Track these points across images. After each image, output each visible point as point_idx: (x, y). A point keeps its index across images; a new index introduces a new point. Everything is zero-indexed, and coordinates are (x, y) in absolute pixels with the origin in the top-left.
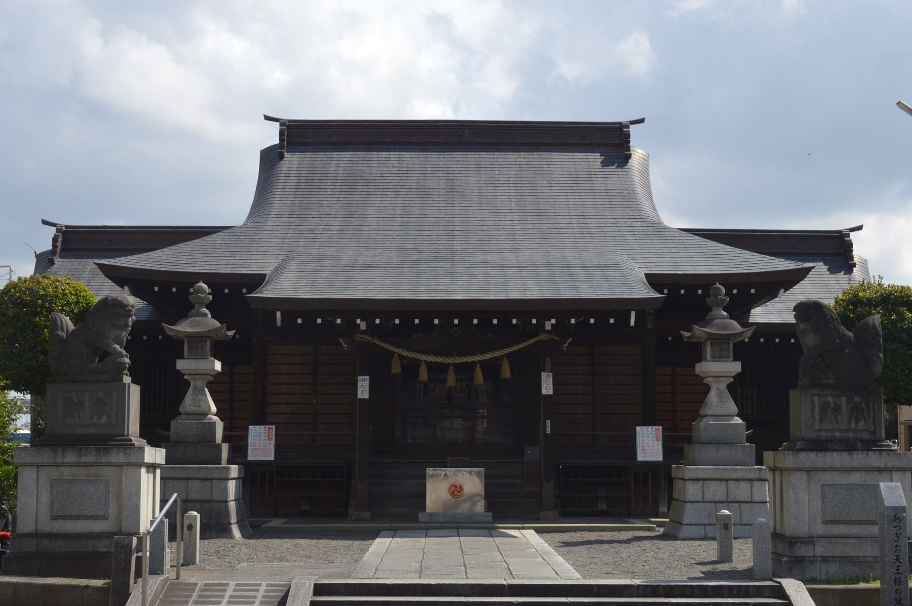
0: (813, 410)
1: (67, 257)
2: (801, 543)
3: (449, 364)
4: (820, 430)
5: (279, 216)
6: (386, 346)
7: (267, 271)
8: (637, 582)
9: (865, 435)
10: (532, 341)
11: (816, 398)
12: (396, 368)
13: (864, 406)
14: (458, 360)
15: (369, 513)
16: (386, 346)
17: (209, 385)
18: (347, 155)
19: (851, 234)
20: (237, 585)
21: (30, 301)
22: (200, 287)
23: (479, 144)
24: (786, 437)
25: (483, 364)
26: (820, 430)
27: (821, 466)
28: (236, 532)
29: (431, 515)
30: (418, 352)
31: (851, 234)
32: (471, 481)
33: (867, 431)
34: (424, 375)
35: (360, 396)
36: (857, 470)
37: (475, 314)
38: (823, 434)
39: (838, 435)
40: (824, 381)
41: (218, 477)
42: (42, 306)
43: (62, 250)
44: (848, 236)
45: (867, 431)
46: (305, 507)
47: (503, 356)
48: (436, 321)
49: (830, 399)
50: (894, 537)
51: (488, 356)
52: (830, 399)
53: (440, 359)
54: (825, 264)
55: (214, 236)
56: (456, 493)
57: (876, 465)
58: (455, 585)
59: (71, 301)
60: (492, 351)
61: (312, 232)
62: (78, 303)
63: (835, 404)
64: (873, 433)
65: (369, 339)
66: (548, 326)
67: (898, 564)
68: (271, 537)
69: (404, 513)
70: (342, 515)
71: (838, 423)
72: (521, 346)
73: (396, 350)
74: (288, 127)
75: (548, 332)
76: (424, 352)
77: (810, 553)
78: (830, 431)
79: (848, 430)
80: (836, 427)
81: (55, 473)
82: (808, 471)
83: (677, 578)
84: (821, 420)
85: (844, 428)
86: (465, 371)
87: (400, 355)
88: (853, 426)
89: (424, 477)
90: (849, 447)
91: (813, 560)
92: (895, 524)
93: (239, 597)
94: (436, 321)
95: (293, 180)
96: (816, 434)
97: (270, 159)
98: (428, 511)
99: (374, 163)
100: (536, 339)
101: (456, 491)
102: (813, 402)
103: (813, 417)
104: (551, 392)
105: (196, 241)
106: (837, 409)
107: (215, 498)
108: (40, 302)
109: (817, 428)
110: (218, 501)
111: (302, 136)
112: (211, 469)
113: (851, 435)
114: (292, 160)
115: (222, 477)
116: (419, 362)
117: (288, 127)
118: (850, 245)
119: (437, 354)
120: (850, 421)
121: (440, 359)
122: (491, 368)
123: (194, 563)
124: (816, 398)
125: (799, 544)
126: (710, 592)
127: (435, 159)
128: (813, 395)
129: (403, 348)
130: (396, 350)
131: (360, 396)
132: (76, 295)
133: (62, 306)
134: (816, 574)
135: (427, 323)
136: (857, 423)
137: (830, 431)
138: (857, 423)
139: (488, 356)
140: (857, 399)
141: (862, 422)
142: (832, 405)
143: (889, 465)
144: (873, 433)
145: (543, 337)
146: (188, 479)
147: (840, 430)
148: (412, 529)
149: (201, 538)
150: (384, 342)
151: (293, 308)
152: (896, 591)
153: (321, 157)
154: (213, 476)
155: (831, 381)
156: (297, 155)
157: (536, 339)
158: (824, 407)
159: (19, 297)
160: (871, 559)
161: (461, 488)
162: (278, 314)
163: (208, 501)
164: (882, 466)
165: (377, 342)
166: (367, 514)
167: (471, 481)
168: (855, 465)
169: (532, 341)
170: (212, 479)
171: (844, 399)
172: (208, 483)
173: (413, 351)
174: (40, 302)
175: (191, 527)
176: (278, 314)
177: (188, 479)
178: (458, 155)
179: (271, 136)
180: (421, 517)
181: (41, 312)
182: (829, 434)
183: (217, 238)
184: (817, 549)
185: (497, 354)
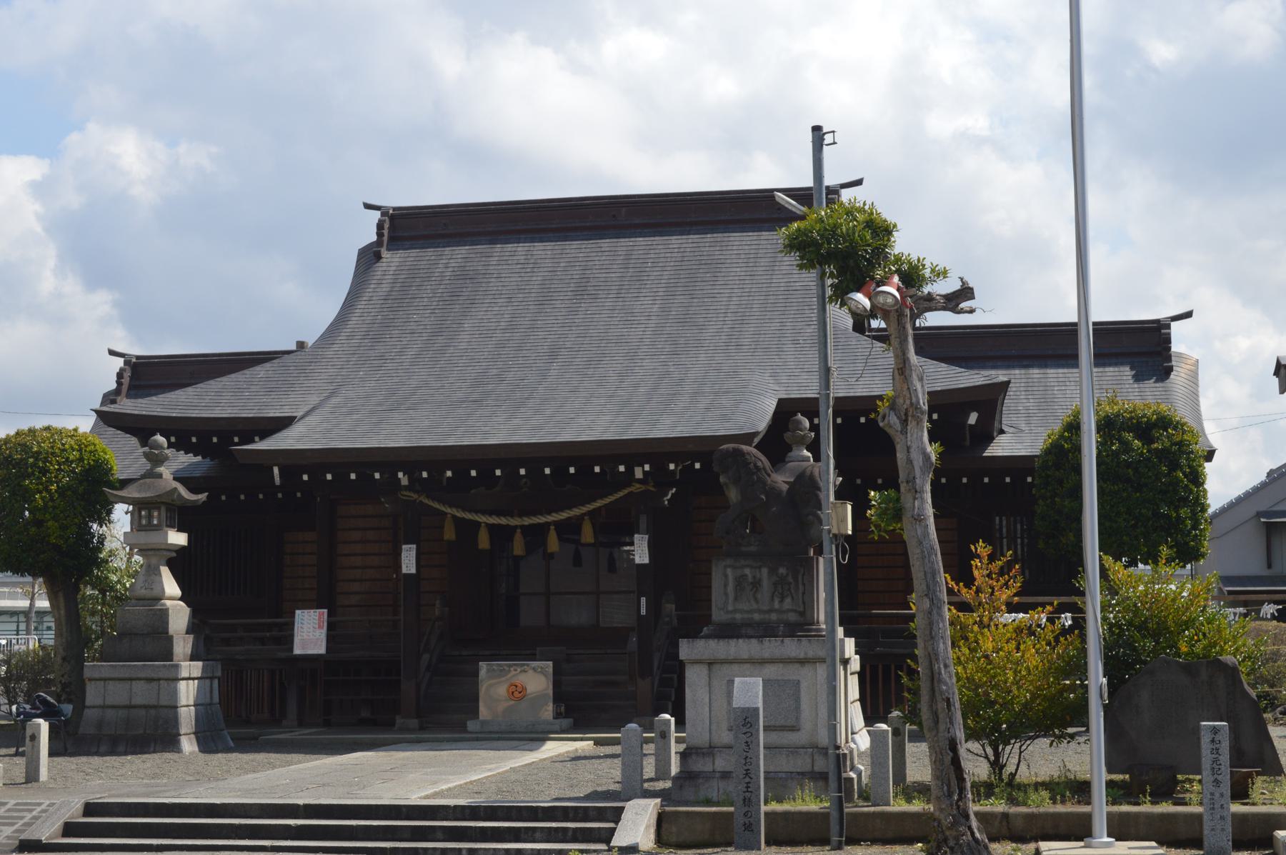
0: (726, 586)
1: (136, 397)
2: (697, 754)
3: (516, 527)
4: (735, 611)
5: (350, 337)
6: (436, 505)
7: (299, 414)
8: (462, 802)
9: (792, 617)
10: (621, 494)
11: (729, 571)
12: (449, 534)
13: (790, 579)
14: (527, 521)
15: (416, 721)
16: (436, 505)
17: (171, 564)
18: (462, 251)
19: (1173, 324)
20: (17, 804)
21: (21, 460)
22: (155, 441)
23: (671, 225)
24: (707, 620)
25: (558, 525)
26: (735, 611)
27: (723, 657)
28: (188, 745)
29: (484, 723)
30: (476, 512)
31: (1173, 324)
32: (536, 679)
33: (795, 611)
34: (484, 541)
35: (404, 570)
36: (772, 661)
37: (352, 467)
38: (738, 616)
39: (757, 617)
40: (744, 549)
41: (166, 676)
42: (34, 465)
43: (130, 388)
44: (1168, 327)
45: (795, 611)
46: (365, 714)
47: (584, 515)
48: (498, 472)
49: (747, 571)
50: (744, 746)
51: (564, 515)
52: (747, 571)
53: (503, 521)
54: (1132, 369)
55: (267, 365)
56: (516, 694)
57: (793, 655)
58: (243, 805)
59: (71, 457)
60: (570, 508)
61: (382, 357)
62: (81, 459)
63: (754, 577)
64: (802, 614)
65: (415, 496)
66: (638, 473)
67: (747, 780)
68: (904, 763)
69: (442, 716)
70: (389, 725)
71: (756, 600)
72: (607, 500)
73: (449, 510)
74: (392, 218)
75: (639, 481)
76: (484, 512)
77: (708, 768)
78: (748, 612)
79: (770, 611)
80: (755, 606)
81: (772, 671)
82: (711, 664)
83: (510, 798)
84: (736, 599)
85: (765, 608)
86: (536, 535)
87: (454, 517)
88: (776, 605)
89: (476, 674)
90: (765, 631)
91: (709, 776)
92: (745, 730)
93: (516, 835)
94: (498, 472)
95: (385, 287)
96: (730, 616)
97: (369, 257)
98: (481, 718)
99: (494, 261)
100: (626, 492)
101: (518, 693)
102: (726, 576)
103: (726, 594)
104: (646, 561)
105: (233, 376)
106: (756, 584)
107: (163, 703)
108: (31, 460)
109: (730, 608)
110: (166, 707)
111: (407, 228)
112: (158, 667)
113: (774, 617)
114: (392, 260)
115: (171, 676)
116: (477, 525)
117: (392, 218)
118: (1168, 340)
119: (499, 513)
120: (772, 599)
121: (503, 521)
122: (568, 530)
123: (36, 779)
124: (729, 571)
125: (694, 757)
126: (540, 815)
127: (576, 250)
128: (726, 567)
129: (457, 507)
130: (449, 510)
131: (404, 570)
132: (80, 450)
133: (59, 464)
134: (714, 795)
135: (486, 475)
136: (782, 601)
137: (748, 612)
138: (782, 601)
139: (564, 515)
140: (782, 571)
141: (788, 600)
142: (750, 579)
143: (811, 654)
144: (802, 614)
145: (636, 488)
146: (131, 679)
147: (760, 611)
148: (456, 740)
149: (52, 753)
150: (433, 499)
151: (294, 461)
152: (745, 815)
153: (430, 253)
154: (161, 675)
155: (753, 549)
156: (401, 253)
157: (626, 492)
158: (740, 582)
159: (10, 456)
160: (784, 775)
161: (524, 689)
162: (276, 470)
163: (154, 707)
164: (802, 656)
165: (426, 501)
166: (414, 723)
167: (536, 679)
168: (766, 655)
169: (621, 494)
170: (159, 679)
171: (765, 571)
172: (154, 684)
173: (470, 511)
174: (31, 460)
175: (34, 738)
176: (276, 470)
177: (131, 679)
178: (606, 244)
179: (366, 230)
180: (471, 725)
181: (33, 474)
182: (746, 616)
183: (260, 371)
184: (717, 762)
185: (576, 512)
